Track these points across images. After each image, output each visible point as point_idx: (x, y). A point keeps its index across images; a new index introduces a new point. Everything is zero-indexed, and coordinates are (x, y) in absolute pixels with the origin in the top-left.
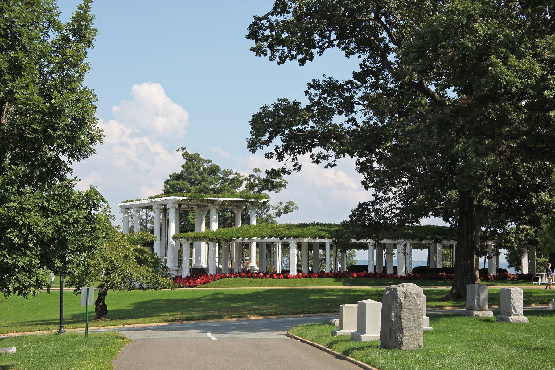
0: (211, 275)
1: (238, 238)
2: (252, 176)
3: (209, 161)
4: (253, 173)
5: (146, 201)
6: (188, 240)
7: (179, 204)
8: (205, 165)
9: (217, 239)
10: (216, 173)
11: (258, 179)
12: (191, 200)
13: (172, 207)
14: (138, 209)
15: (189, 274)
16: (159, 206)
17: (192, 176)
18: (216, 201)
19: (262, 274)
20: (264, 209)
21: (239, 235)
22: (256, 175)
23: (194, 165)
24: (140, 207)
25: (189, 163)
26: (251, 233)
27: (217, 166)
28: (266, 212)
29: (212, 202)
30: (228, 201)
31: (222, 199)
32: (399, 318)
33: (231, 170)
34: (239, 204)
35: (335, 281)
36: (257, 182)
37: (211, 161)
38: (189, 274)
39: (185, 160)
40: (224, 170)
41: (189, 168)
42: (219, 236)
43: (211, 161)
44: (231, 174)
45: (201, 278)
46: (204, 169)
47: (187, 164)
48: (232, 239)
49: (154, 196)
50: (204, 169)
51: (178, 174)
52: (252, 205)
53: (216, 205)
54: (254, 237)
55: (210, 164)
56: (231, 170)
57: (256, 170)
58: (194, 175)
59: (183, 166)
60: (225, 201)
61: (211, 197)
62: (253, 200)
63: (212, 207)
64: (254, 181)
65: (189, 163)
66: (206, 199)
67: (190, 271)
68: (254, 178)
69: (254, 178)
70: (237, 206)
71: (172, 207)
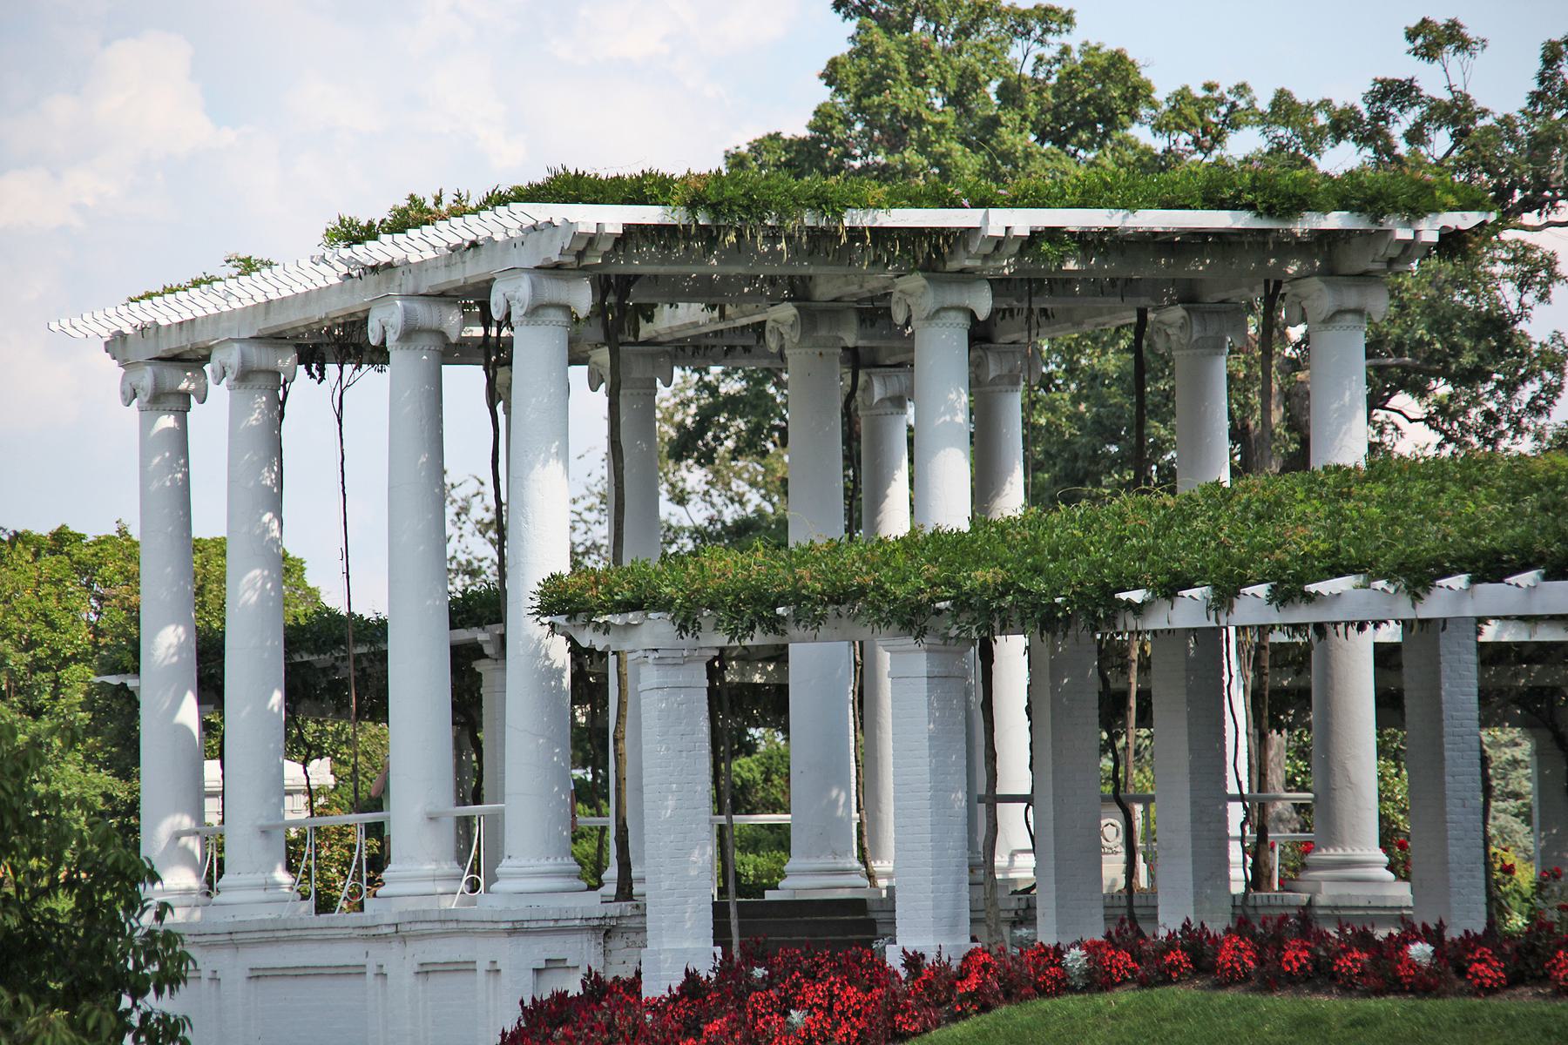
0: (913, 961)
1: (1171, 588)
2: (1395, 92)
3: (1046, 15)
4: (1403, 65)
5: (304, 275)
6: (687, 624)
7: (603, 285)
8: (1022, 56)
9: (962, 603)
10: (1110, 121)
11: (1456, 113)
12: (710, 236)
13: (536, 310)
14: (261, 357)
15: (703, 957)
16: (425, 314)
17: (911, 155)
18: (967, 234)
19: (1420, 951)
20: (1510, 387)
21: (1186, 561)
22: (1433, 80)
23: (916, 57)
24: (275, 339)
25: (882, 42)
26: (1305, 534)
27: (1118, 60)
28: (1535, 408)
29: (932, 253)
30: (1086, 241)
31: (1022, 221)
32: (1188, 678)
33: (1242, 89)
34: (1199, 267)
35: (504, 1034)
36: (1441, 142)
37: (1068, 19)
38: (703, 957)
39: (851, 26)
40: (1183, 95)
41: (876, 82)
42: (985, 575)
43: (1068, 19)
44: (1234, 121)
45: (815, 993)
46: (1011, 94)
47: (864, 49)
48: (1107, 592)
49: (379, 212)
50: (1011, 94)
51: (789, 145)
52: (1330, 272)
53: (966, 277)
54: (1335, 571)
55: (1054, 43)
56: (1242, 89)
57: (1435, 39)
58: (923, 146)
59: (832, 74)
60: (1053, 234)
61: (916, 201)
62: (1335, 220)
63: (929, 301)
64: (1415, 136)
65: (882, 42)
66: (855, 218)
67: (721, 934)
68: (1412, 115)
69: (1412, 115)
70: (1189, 297)
71: (536, 310)
